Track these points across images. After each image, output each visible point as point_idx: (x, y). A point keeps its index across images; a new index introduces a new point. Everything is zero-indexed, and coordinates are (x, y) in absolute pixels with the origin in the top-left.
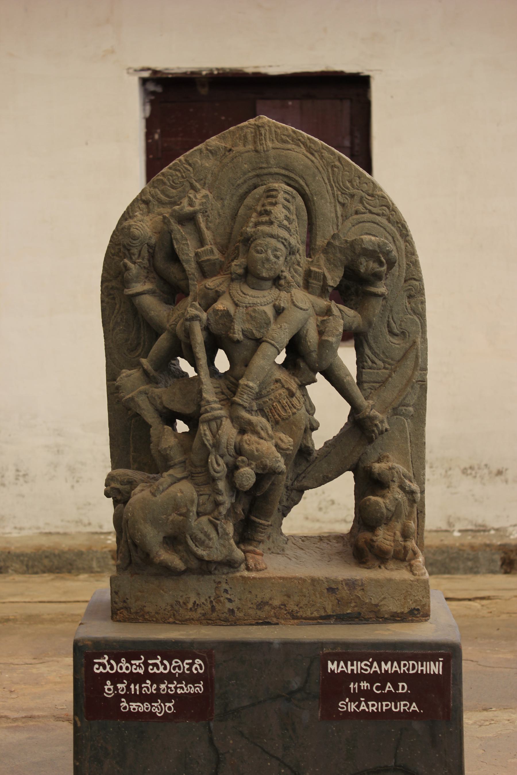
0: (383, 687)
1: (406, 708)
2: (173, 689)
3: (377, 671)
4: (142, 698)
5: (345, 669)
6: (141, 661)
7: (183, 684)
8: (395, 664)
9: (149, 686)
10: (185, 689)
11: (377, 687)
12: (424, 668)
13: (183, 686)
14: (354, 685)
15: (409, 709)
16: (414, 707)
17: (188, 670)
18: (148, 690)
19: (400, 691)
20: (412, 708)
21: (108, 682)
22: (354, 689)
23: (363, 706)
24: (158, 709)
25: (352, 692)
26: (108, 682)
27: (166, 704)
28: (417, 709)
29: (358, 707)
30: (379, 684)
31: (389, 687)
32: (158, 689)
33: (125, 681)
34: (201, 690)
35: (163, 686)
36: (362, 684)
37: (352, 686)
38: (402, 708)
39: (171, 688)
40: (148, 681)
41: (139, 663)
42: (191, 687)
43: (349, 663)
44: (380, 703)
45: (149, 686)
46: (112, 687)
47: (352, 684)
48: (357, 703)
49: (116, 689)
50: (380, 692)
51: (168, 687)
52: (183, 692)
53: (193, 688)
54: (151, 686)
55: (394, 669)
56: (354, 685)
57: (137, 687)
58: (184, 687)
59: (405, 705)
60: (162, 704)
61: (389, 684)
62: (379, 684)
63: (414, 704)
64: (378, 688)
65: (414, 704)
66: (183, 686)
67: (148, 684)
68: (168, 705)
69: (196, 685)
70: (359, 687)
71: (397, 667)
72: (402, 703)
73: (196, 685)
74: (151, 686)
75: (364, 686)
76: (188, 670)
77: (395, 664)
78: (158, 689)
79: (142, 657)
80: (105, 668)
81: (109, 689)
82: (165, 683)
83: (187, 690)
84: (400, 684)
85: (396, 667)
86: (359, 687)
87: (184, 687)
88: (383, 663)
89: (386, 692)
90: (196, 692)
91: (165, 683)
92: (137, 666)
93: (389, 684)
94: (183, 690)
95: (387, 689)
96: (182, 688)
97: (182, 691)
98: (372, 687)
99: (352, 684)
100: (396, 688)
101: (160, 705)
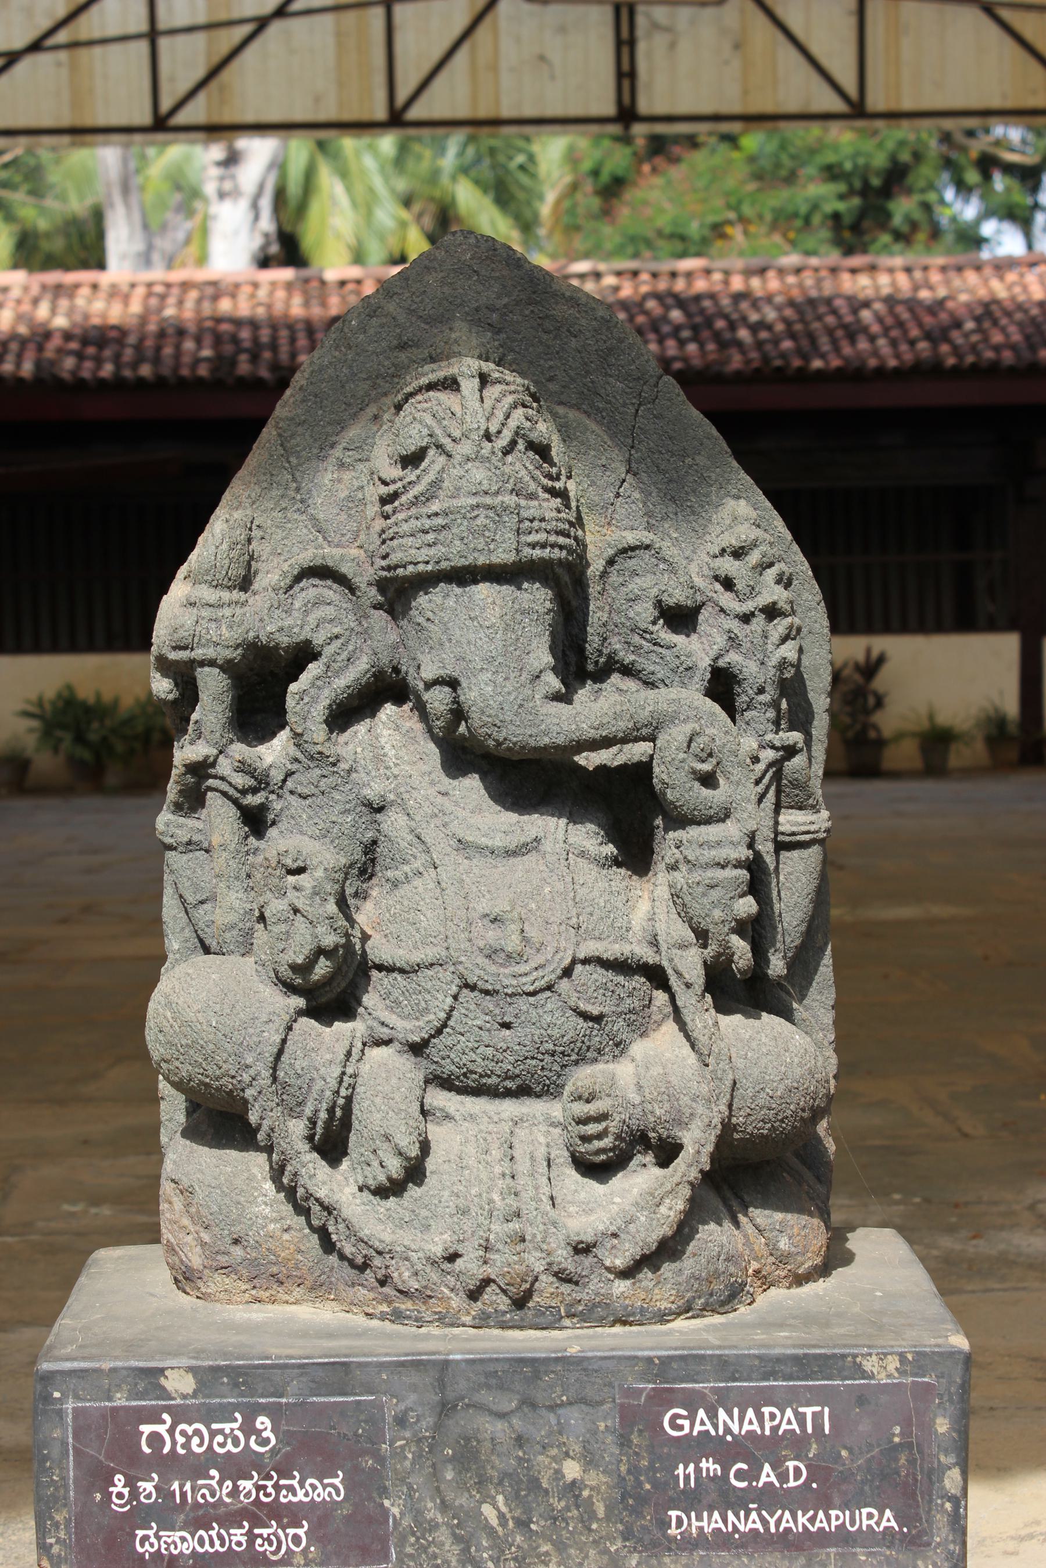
0: (752, 1474)
1: (872, 1522)
2: (270, 1490)
3: (707, 1431)
4: (200, 1519)
5: (756, 1427)
6: (236, 1425)
7: (294, 1478)
8: (750, 1413)
9: (214, 1483)
10: (301, 1493)
11: (739, 1470)
12: (705, 1524)
13: (295, 1483)
14: (686, 1468)
15: (878, 1524)
16: (889, 1520)
17: (183, 1446)
18: (213, 1495)
19: (792, 1484)
20: (884, 1524)
21: (119, 1479)
22: (687, 1477)
23: (754, 1522)
24: (271, 1544)
25: (682, 1485)
26: (119, 1479)
27: (288, 1531)
28: (893, 1524)
29: (812, 1520)
30: (745, 1467)
31: (767, 1475)
32: (235, 1492)
33: (154, 1475)
34: (338, 1495)
35: (246, 1485)
36: (704, 1464)
37: (680, 1470)
38: (865, 1523)
39: (265, 1487)
40: (213, 1472)
41: (232, 1430)
42: (314, 1487)
43: (693, 1514)
44: (847, 1513)
45: (214, 1483)
46: (126, 1491)
47: (681, 1466)
48: (811, 1513)
49: (135, 1493)
50: (743, 1485)
51: (259, 1488)
52: (295, 1500)
53: (320, 1489)
54: (220, 1483)
55: (746, 1427)
56: (686, 1468)
57: (188, 1487)
58: (297, 1486)
59: (870, 1516)
60: (222, 1531)
61: (767, 1468)
62: (745, 1467)
63: (888, 1513)
64: (739, 1475)
65: (888, 1513)
66: (295, 1483)
67: (213, 1478)
68: (291, 1531)
69: (326, 1481)
70: (698, 1470)
71: (754, 1420)
72: (865, 1511)
73: (326, 1481)
74: (220, 1483)
75: (708, 1469)
76: (183, 1446)
77: (750, 1413)
78: (235, 1492)
79: (237, 1415)
80: (236, 1442)
81: (120, 1496)
82: (252, 1478)
83: (306, 1494)
84: (791, 1464)
85: (751, 1423)
86: (698, 1470)
87: (297, 1486)
88: (730, 1514)
89: (760, 1485)
90: (202, 1501)
91: (252, 1478)
92: (226, 1437)
93: (767, 1468)
94: (295, 1494)
95: (763, 1479)
96: (291, 1489)
97: (290, 1497)
98: (726, 1470)
99: (681, 1466)
100: (783, 1477)
101: (275, 1534)
